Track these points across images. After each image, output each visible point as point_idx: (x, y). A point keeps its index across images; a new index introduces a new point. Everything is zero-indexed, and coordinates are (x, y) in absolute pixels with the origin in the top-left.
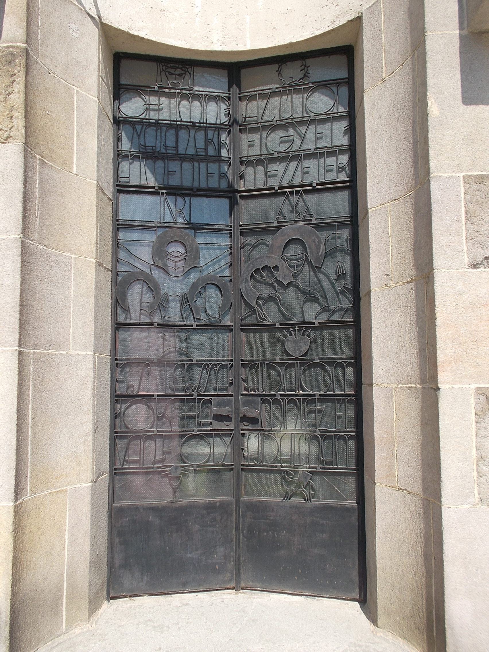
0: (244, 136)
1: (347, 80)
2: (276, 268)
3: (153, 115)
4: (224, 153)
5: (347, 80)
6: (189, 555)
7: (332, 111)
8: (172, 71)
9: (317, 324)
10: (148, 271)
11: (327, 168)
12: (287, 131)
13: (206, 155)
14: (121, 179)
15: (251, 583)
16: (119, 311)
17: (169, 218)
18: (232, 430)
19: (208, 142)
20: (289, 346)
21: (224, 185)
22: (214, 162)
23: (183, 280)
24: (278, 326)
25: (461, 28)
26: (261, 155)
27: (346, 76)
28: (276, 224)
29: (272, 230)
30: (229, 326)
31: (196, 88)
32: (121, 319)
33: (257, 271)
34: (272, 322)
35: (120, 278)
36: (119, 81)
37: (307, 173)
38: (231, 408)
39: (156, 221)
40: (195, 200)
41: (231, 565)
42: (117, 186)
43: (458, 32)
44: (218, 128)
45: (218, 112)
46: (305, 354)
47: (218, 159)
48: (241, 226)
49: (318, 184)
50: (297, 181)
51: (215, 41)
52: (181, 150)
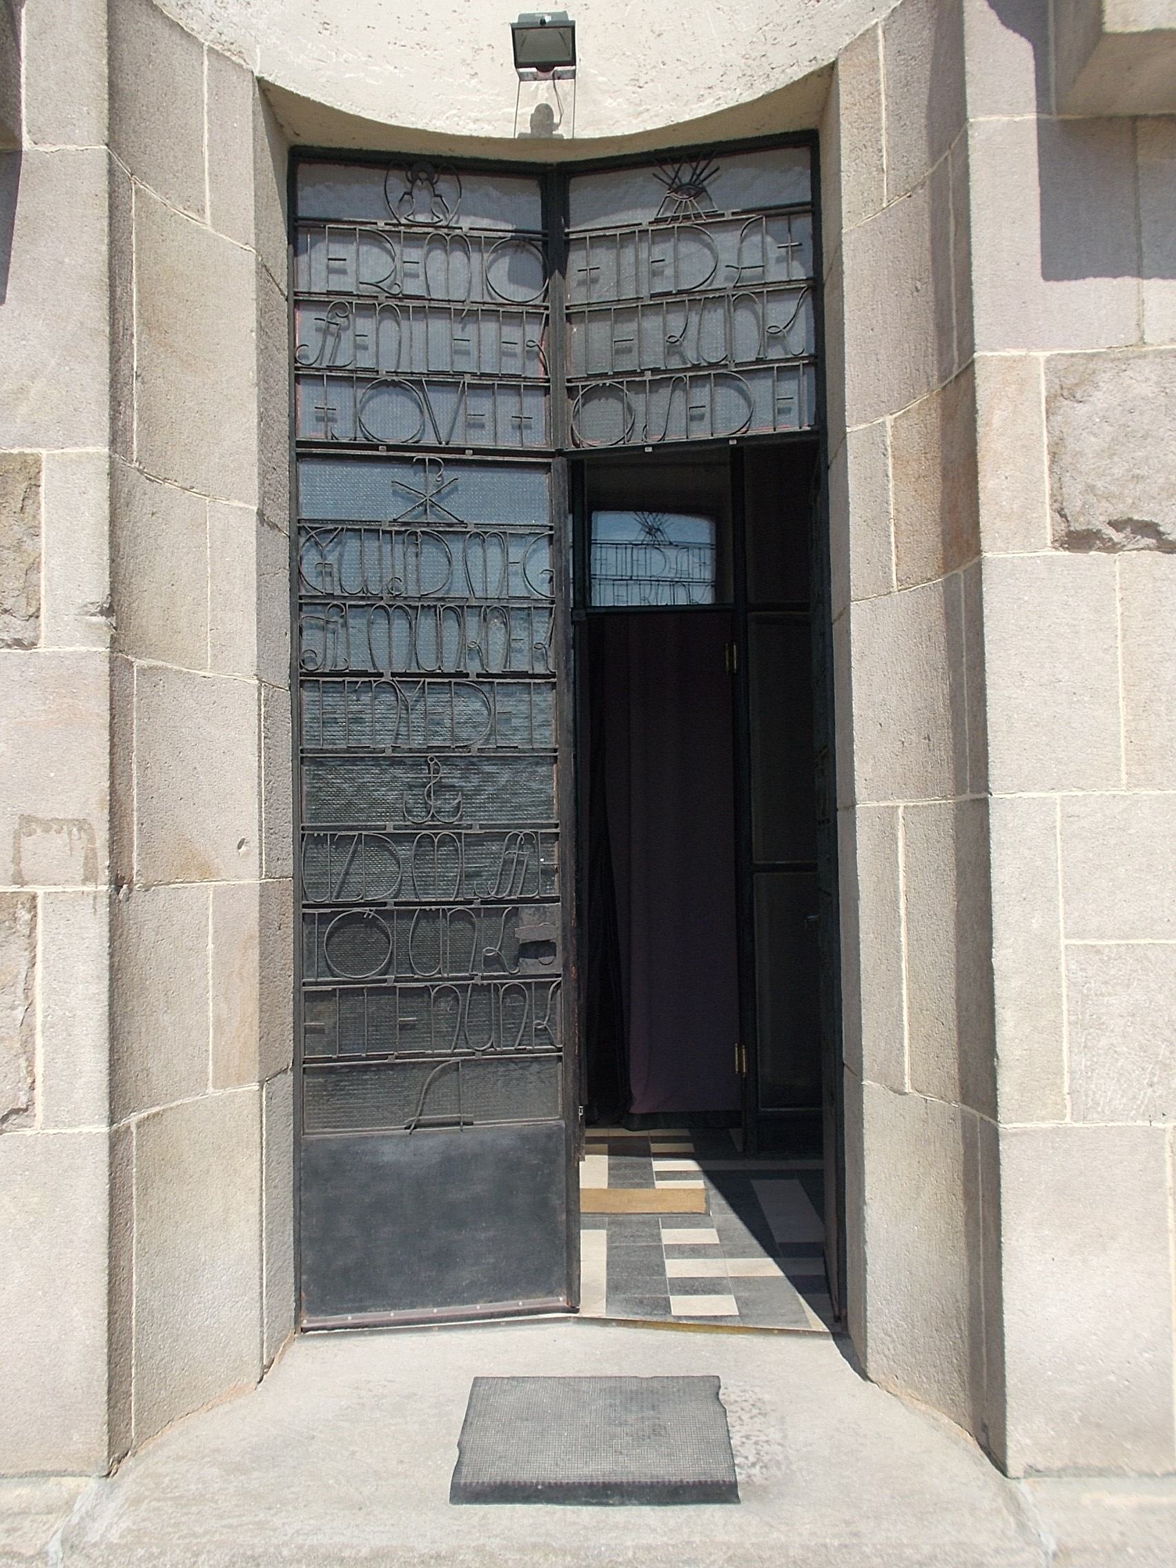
1: (809, 207)
5: (809, 207)
7: (710, 285)
25: (1042, 107)
27: (808, 198)
43: (1032, 117)
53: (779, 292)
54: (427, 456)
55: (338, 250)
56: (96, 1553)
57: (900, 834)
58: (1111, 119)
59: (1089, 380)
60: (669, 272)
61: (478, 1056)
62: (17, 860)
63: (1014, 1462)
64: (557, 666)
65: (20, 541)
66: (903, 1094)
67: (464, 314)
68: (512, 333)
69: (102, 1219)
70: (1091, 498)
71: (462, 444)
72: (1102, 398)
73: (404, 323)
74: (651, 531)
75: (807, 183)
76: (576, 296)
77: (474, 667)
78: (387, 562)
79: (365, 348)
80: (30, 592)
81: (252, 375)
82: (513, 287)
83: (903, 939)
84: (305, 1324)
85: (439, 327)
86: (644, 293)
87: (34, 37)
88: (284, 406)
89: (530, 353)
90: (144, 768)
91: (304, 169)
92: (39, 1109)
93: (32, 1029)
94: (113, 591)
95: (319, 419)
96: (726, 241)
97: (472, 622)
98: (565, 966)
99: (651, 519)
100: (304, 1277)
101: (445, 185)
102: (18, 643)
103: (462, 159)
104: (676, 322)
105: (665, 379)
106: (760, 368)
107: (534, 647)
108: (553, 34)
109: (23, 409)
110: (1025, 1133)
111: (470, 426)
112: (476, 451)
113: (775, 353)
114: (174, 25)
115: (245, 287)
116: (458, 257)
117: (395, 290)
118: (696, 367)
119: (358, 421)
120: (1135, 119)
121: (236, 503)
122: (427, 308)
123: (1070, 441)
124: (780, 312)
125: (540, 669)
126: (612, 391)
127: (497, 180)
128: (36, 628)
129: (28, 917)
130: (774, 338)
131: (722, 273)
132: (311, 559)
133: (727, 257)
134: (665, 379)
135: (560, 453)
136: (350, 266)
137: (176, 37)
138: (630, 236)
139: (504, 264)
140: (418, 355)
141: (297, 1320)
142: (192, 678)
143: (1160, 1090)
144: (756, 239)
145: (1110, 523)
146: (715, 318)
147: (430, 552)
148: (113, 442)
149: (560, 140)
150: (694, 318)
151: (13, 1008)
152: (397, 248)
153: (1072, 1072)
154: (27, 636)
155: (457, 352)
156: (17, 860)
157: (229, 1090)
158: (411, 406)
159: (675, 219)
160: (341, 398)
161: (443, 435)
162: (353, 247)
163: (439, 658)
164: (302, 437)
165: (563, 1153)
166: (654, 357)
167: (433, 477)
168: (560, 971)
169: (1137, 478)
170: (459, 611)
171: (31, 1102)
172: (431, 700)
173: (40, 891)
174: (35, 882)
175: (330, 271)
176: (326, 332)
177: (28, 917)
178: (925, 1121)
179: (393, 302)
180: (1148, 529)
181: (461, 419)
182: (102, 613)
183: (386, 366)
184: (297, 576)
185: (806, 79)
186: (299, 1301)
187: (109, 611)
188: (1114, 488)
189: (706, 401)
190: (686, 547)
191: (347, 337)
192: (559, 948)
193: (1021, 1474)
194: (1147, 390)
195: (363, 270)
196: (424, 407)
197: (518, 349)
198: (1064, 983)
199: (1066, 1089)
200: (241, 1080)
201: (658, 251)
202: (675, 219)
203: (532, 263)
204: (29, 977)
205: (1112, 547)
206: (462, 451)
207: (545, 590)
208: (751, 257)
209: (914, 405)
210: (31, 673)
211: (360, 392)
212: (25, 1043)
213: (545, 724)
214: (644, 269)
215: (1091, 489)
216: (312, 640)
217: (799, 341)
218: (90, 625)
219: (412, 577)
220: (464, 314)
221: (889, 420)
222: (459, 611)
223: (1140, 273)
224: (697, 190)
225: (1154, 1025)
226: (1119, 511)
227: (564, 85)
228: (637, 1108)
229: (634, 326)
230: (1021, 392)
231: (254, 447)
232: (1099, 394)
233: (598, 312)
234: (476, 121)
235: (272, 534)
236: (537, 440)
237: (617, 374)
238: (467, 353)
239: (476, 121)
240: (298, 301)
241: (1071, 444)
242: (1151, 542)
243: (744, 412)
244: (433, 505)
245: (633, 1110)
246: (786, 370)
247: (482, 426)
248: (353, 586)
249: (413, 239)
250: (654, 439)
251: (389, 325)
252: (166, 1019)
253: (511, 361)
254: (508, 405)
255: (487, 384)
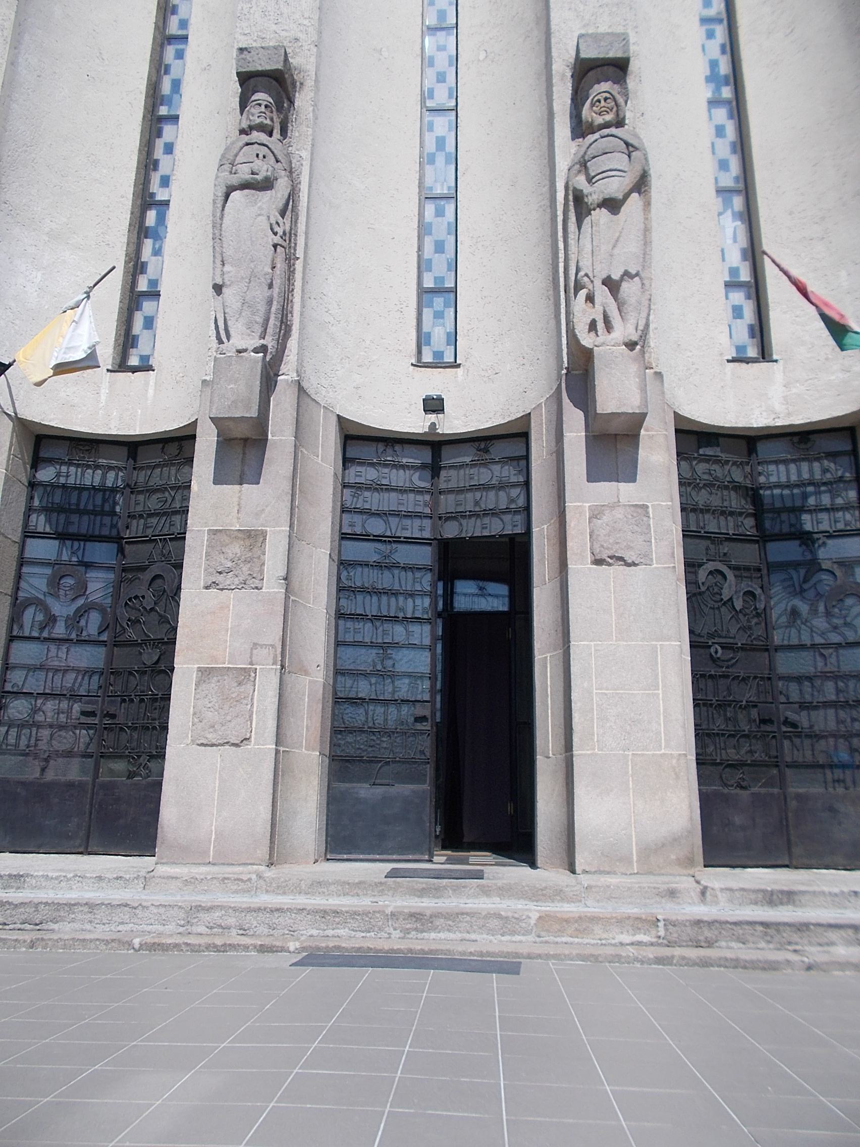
0: (133, 496)
2: (143, 597)
3: (62, 480)
4: (118, 509)
6: (47, 822)
8: (81, 447)
9: (166, 640)
10: (42, 597)
11: (514, 524)
12: (164, 493)
13: (102, 510)
14: (30, 528)
15: (95, 848)
16: (15, 627)
17: (65, 557)
18: (96, 724)
19: (104, 501)
20: (145, 657)
21: (114, 533)
22: (108, 515)
23: (70, 605)
24: (139, 641)
26: (687, 504)
28: (147, 563)
29: (143, 569)
30: (106, 642)
31: (100, 461)
32: (15, 633)
33: (130, 600)
34: (135, 639)
35: (18, 601)
36: (38, 455)
37: (173, 525)
38: (98, 706)
39: (53, 559)
40: (88, 544)
41: (82, 833)
42: (25, 532)
44: (114, 490)
45: (116, 478)
46: (157, 662)
47: (113, 513)
48: (124, 564)
49: (178, 534)
50: (165, 531)
51: (112, 427)
52: (82, 507)
53: (514, 485)
54: (387, 539)
55: (359, 469)
56: (267, 880)
57: (548, 666)
58: (608, 435)
59: (602, 513)
60: (476, 478)
61: (398, 759)
62: (251, 658)
63: (578, 869)
64: (432, 616)
65: (260, 556)
66: (549, 757)
67: (402, 491)
68: (419, 498)
69: (272, 777)
70: (602, 549)
71: (400, 535)
72: (606, 518)
73: (381, 494)
74: (481, 589)
75: (525, 449)
76: (443, 486)
77: (401, 615)
78: (371, 575)
79: (367, 502)
80: (261, 572)
81: (330, 509)
82: (420, 482)
83: (549, 702)
84: (328, 857)
85: (393, 495)
86: (467, 485)
87: (276, 406)
88: (338, 521)
89: (426, 505)
90: (291, 633)
91: (349, 442)
92: (253, 739)
93: (253, 712)
94: (287, 573)
95: (350, 526)
96: (496, 468)
97: (401, 599)
98: (432, 727)
99: (481, 584)
100: (329, 839)
101: (398, 447)
102: (257, 588)
103: (404, 439)
104: (478, 495)
105: (474, 515)
106: (508, 511)
107: (424, 609)
108: (438, 402)
109: (263, 516)
110: (582, 755)
111: (403, 529)
112: (405, 538)
113: (513, 506)
114: (314, 400)
115: (330, 480)
116: (401, 472)
117: (379, 483)
118: (484, 510)
119: (363, 526)
120: (616, 435)
121: (323, 550)
122: (389, 489)
123: (596, 531)
124: (515, 492)
125: (425, 617)
126: (455, 518)
127: (416, 446)
128: (263, 583)
129: (254, 675)
130: (512, 501)
131: (495, 478)
132: (344, 574)
133: (497, 473)
134: (474, 515)
135: (435, 539)
136: (363, 474)
137: (314, 403)
138: (463, 466)
139: (417, 474)
140: (386, 504)
141: (326, 854)
142: (307, 606)
143: (627, 742)
144: (507, 467)
145: (609, 557)
146: (492, 494)
147: (387, 573)
148: (290, 527)
149: (438, 433)
150: (484, 494)
151: (247, 705)
152: (380, 468)
153: (598, 734)
154: (259, 586)
155: (399, 504)
156: (251, 658)
157: (310, 752)
158: (382, 521)
159: (478, 460)
160: (358, 519)
161: (393, 532)
162: (364, 468)
163: (389, 611)
164: (343, 532)
165: (429, 799)
166: (470, 507)
167: (389, 547)
168: (429, 729)
169: (617, 543)
170: (396, 594)
171: (251, 736)
172: (385, 625)
173: (258, 667)
174: (257, 664)
175: (357, 476)
176: (354, 496)
177: (254, 675)
178: (556, 765)
179: (377, 487)
180: (621, 559)
181: (399, 528)
182: (284, 579)
183: (374, 508)
184: (339, 579)
185: (522, 417)
186: (326, 847)
187: (285, 579)
188: (610, 546)
189: (488, 522)
190: (497, 596)
191: (361, 498)
192: (430, 720)
193: (580, 872)
194: (620, 516)
195: (367, 476)
196: (387, 522)
197: (421, 503)
198: (595, 705)
199: (596, 740)
200: (314, 750)
201: (472, 471)
202: (478, 460)
203: (428, 474)
204: (253, 695)
205: (610, 565)
206: (400, 537)
207: (429, 588)
208: (505, 473)
209: (552, 521)
210: (260, 598)
211: (364, 517)
212: (250, 717)
213: (427, 637)
214: (467, 477)
215: (602, 546)
216: (343, 602)
217: (521, 502)
218: (280, 583)
219: (380, 582)
220: (402, 491)
221: (545, 526)
222: (396, 594)
223: (618, 481)
224: (486, 451)
225: (625, 719)
226: (610, 553)
227: (441, 416)
228: (465, 840)
229: (463, 496)
230: (580, 516)
231: (330, 532)
232: (605, 517)
233: (450, 491)
234: (409, 427)
235: (333, 563)
236: (427, 534)
237: (456, 512)
238: (403, 504)
239: (409, 427)
240: (345, 486)
241: (596, 532)
242: (623, 563)
243: (502, 526)
244: (389, 556)
245: (465, 840)
246: (516, 512)
247: (407, 529)
248: (359, 584)
249: (386, 466)
250: (469, 535)
251: (376, 494)
252: (292, 720)
253: (419, 507)
254: (417, 522)
255: (409, 515)
